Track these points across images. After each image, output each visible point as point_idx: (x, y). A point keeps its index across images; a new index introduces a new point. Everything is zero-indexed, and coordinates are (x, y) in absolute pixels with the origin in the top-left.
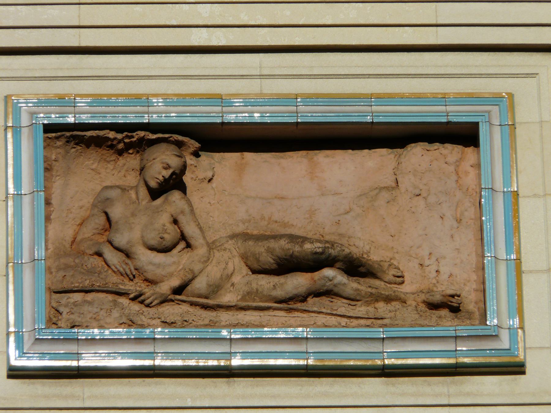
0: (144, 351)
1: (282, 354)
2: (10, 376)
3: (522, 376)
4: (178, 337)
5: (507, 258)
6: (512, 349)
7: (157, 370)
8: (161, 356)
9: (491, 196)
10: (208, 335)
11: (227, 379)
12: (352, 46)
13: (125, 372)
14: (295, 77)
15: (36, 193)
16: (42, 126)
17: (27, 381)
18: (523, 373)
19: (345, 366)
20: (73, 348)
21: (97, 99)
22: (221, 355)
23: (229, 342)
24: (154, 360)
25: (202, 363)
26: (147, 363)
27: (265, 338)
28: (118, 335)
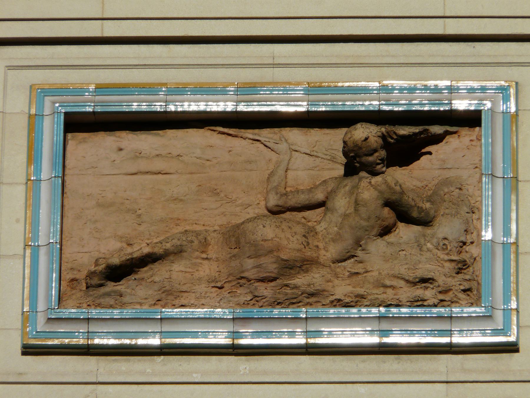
0: (313, 330)
1: (144, 334)
2: (24, 353)
3: (516, 355)
4: (138, 317)
5: (504, 241)
6: (506, 329)
7: (164, 349)
8: (377, 334)
9: (490, 182)
10: (143, 315)
11: (396, 356)
12: (475, 35)
13: (377, 349)
14: (455, 65)
15: (53, 179)
16: (63, 115)
17: (243, 358)
18: (517, 351)
19: (176, 344)
20: (445, 326)
21: (101, 88)
22: (66, 334)
23: (305, 321)
24: (451, 337)
25: (127, 342)
26: (445, 340)
27: (227, 319)
28: (193, 315)
